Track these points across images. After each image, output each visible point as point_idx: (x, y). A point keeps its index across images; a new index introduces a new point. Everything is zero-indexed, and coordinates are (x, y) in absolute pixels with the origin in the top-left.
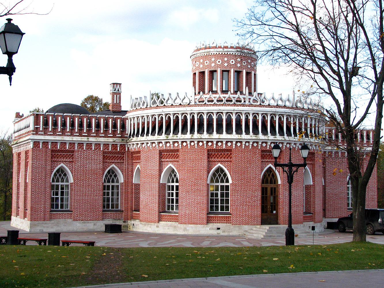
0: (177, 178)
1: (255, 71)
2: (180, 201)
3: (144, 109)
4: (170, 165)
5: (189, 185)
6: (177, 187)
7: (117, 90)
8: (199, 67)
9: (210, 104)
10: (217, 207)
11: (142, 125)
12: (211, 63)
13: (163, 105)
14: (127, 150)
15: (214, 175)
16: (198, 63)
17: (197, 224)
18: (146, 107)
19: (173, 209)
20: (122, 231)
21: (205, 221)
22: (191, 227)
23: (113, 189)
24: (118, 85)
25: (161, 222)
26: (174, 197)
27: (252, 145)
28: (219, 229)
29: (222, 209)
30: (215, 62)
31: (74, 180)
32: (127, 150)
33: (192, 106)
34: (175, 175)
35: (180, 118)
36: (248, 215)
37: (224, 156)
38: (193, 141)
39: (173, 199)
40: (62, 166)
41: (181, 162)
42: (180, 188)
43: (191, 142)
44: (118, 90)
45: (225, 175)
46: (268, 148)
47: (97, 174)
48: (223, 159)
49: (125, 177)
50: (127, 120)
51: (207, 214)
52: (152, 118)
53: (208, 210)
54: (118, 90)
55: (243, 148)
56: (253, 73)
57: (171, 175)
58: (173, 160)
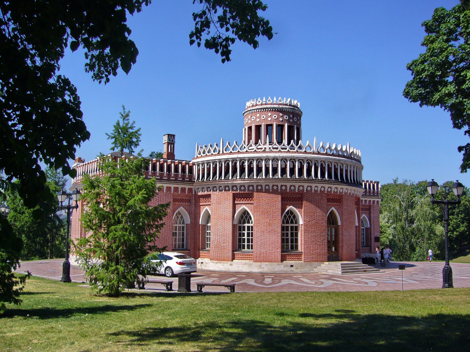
1: (300, 124)
3: (215, 155)
4: (244, 207)
5: (264, 226)
7: (171, 140)
8: (266, 119)
9: (251, 152)
11: (202, 171)
12: (268, 117)
14: (194, 193)
16: (254, 117)
17: (272, 262)
18: (219, 153)
19: (244, 248)
21: (280, 259)
22: (267, 265)
23: (179, 230)
25: (234, 260)
27: (273, 188)
28: (292, 266)
30: (260, 117)
32: (194, 193)
33: (268, 152)
34: (182, 217)
36: (318, 253)
38: (221, 186)
39: (287, 239)
41: (255, 204)
44: (172, 141)
45: (251, 218)
46: (297, 191)
48: (335, 204)
50: (194, 166)
54: (172, 141)
55: (313, 192)
56: (295, 126)
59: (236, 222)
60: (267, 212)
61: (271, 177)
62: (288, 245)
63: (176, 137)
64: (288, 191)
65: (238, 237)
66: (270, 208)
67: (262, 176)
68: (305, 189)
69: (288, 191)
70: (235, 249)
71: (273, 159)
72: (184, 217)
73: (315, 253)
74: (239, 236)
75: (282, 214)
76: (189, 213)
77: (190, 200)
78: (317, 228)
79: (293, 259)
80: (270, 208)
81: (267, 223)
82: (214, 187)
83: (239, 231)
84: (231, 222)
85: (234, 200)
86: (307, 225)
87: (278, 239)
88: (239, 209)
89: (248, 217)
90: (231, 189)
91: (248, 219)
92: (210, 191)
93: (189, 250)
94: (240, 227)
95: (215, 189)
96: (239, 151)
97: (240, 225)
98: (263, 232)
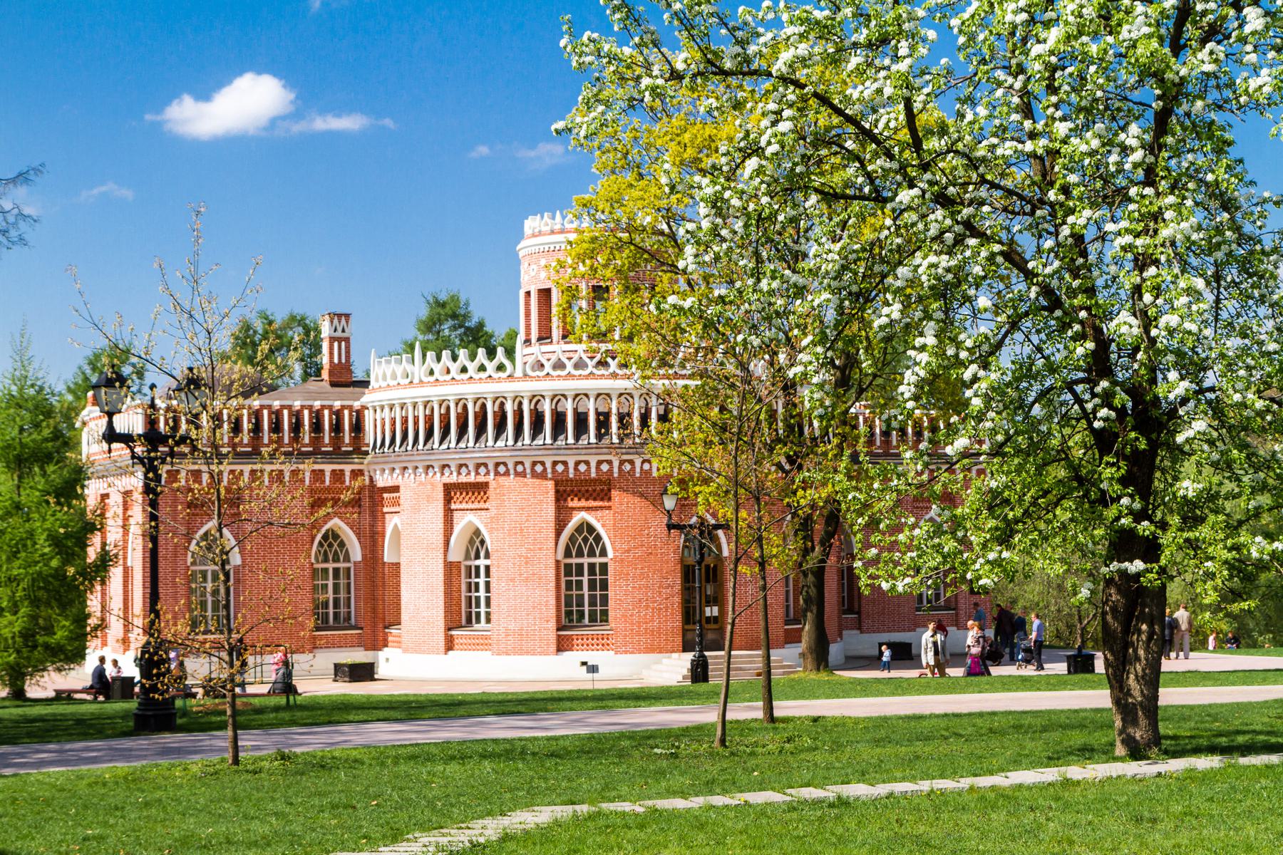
0: (487, 549)
2: (493, 603)
3: (405, 387)
5: (514, 564)
6: (487, 568)
7: (340, 329)
9: (559, 376)
10: (581, 614)
13: (543, 373)
15: (572, 539)
19: (478, 621)
20: (376, 676)
21: (553, 647)
24: (343, 318)
25: (450, 652)
26: (482, 593)
29: (593, 619)
31: (243, 560)
34: (482, 542)
35: (509, 408)
36: (653, 631)
37: (595, 495)
40: (335, 525)
41: (493, 512)
42: (492, 570)
43: (517, 463)
45: (598, 538)
47: (297, 543)
49: (363, 547)
50: (366, 412)
51: (558, 630)
52: (425, 407)
53: (558, 620)
55: (638, 475)
57: (471, 542)
58: (476, 505)
59: (456, 555)
60: (521, 530)
61: (527, 441)
62: (327, 614)
63: (352, 319)
64: (571, 476)
65: (464, 594)
66: (527, 520)
67: (567, 439)
68: (616, 470)
69: (571, 476)
70: (451, 625)
71: (599, 395)
72: (348, 545)
73: (646, 629)
74: (567, 590)
75: (558, 534)
76: (358, 535)
77: (360, 499)
78: (649, 567)
79: (588, 647)
80: (527, 520)
81: (520, 556)
82: (461, 466)
83: (565, 576)
84: (441, 556)
85: (448, 500)
86: (622, 560)
87: (547, 596)
88: (463, 521)
89: (478, 543)
90: (512, 471)
91: (336, 551)
92: (488, 473)
93: (361, 629)
94: (568, 567)
95: (502, 469)
96: (591, 373)
97: (569, 561)
98: (513, 580)
